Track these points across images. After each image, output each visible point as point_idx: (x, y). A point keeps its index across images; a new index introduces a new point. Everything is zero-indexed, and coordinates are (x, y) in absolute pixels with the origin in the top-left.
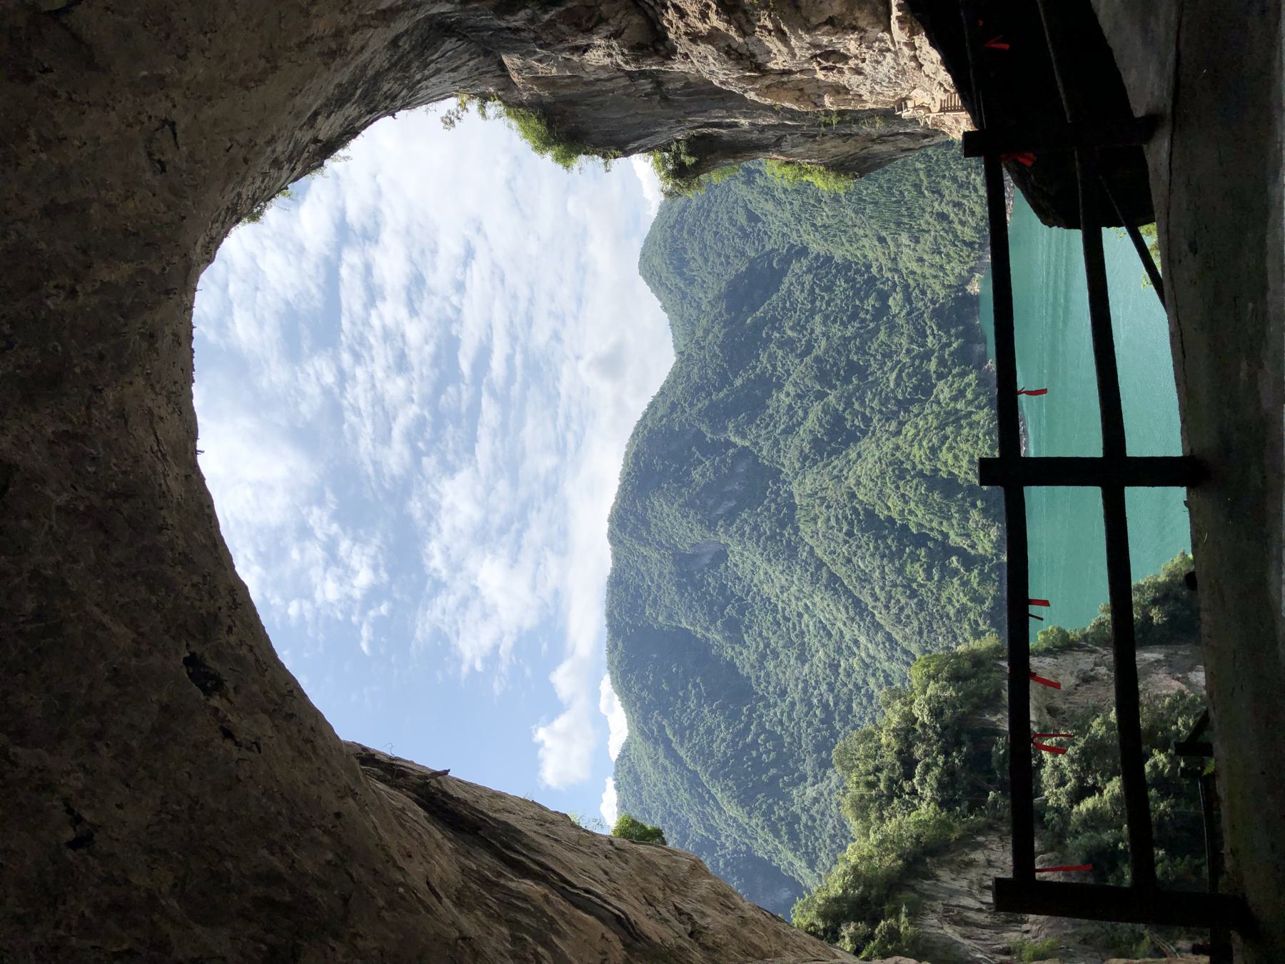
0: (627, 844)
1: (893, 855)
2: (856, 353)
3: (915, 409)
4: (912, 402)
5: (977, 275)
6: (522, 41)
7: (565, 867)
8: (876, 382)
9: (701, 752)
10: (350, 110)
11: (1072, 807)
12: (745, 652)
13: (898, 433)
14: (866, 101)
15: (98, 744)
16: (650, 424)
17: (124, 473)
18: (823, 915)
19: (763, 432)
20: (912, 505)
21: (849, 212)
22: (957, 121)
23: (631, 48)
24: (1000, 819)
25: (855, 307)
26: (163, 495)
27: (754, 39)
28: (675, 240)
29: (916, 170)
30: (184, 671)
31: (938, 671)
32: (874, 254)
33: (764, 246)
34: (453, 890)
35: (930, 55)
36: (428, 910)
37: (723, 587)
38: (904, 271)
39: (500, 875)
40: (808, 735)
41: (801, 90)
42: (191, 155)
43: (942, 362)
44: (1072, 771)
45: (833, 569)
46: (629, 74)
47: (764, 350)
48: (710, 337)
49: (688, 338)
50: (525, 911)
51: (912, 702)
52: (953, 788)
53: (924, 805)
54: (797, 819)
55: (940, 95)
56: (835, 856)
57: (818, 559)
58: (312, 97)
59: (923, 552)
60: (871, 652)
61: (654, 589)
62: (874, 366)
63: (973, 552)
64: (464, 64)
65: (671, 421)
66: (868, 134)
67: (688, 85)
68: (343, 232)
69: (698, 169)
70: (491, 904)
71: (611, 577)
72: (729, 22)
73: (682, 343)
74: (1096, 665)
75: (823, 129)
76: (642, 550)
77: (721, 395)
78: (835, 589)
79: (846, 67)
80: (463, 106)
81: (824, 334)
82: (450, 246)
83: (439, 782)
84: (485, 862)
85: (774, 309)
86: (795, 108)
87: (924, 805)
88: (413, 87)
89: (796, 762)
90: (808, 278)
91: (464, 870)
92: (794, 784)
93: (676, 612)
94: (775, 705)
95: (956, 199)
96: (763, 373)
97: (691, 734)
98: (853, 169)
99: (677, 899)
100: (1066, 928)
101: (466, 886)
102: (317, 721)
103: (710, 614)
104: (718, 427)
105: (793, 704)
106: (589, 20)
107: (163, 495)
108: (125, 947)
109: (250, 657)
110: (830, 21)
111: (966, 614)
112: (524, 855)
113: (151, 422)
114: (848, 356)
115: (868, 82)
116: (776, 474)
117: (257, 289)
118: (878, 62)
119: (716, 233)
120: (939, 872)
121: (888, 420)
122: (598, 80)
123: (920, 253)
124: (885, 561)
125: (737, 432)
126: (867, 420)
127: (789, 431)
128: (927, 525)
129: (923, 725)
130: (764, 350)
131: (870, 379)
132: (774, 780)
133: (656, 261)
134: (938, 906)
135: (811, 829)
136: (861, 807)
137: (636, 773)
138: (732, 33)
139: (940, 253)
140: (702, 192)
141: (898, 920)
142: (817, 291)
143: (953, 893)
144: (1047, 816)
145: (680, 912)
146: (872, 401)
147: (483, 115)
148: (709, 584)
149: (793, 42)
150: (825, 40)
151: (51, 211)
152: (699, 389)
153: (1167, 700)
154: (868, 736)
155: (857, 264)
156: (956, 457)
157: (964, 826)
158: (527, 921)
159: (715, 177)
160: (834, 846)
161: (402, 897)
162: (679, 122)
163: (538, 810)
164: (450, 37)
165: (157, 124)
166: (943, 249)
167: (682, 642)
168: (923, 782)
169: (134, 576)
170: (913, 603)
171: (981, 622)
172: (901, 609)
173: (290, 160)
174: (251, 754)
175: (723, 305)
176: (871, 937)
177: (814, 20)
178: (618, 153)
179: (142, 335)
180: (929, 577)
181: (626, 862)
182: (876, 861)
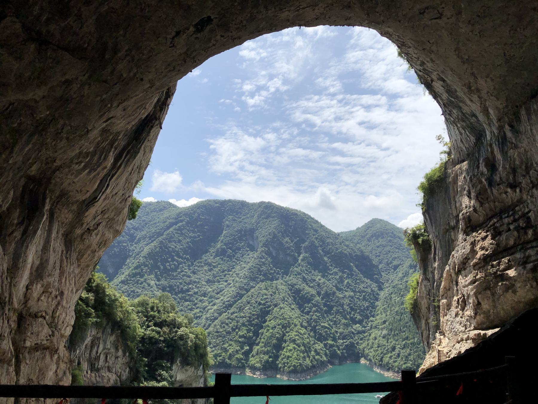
0: (128, 204)
3: (312, 334)
4: (315, 332)
5: (368, 363)
6: (473, 170)
7: (119, 176)
8: (324, 317)
9: (171, 237)
10: (445, 96)
12: (212, 257)
14: (443, 318)
18: (98, 286)
19: (304, 269)
20: (271, 331)
21: (397, 309)
22: (434, 357)
24: (136, 363)
25: (356, 310)
27: (472, 270)
29: (414, 338)
30: (205, 16)
31: (199, 339)
32: (379, 319)
34: (109, 128)
35: (464, 347)
36: (101, 116)
37: (239, 249)
38: (371, 331)
39: (116, 149)
41: (449, 290)
43: (331, 346)
46: (458, 216)
47: (339, 270)
49: (345, 238)
51: (187, 327)
52: (149, 344)
53: (143, 331)
54: (142, 276)
55: (445, 350)
56: (126, 292)
57: (250, 290)
58: (451, 78)
60: (210, 311)
61: (240, 220)
62: (331, 317)
64: (464, 145)
66: (430, 318)
67: (453, 241)
68: (393, 96)
69: (416, 244)
70: (103, 144)
71: (245, 202)
72: (480, 259)
75: (432, 299)
76: (256, 215)
77: (321, 251)
78: (237, 296)
79: (459, 309)
81: (345, 296)
82: (387, 141)
83: (157, 125)
84: (122, 142)
86: (442, 287)
88: (454, 123)
89: (165, 278)
91: (118, 133)
92: (156, 276)
93: (230, 228)
94: (190, 269)
95: (401, 355)
96: (329, 269)
97: (179, 233)
99: (104, 223)
101: (111, 134)
104: (307, 249)
105: (189, 277)
106: (482, 198)
109: (211, 45)
110: (479, 304)
111: (224, 352)
113: (312, 5)
114: (335, 306)
115: (452, 319)
116: (286, 273)
117: (370, 61)
118: (461, 324)
119: (389, 252)
120: (114, 335)
121: (308, 322)
122: (456, 202)
123: (378, 338)
124: (248, 318)
126: (308, 313)
127: (304, 280)
128: (263, 337)
129: (177, 332)
130: (339, 270)
131: (325, 315)
132: (158, 268)
133: (378, 225)
134: (100, 335)
136: (143, 304)
138: (475, 261)
139: (378, 347)
140: (406, 245)
141: (94, 317)
142: (364, 294)
143: (105, 342)
145: (98, 225)
146: (316, 315)
147: (442, 153)
148: (241, 243)
149: (470, 287)
150: (471, 301)
152: (323, 242)
154: (173, 308)
155: (375, 311)
156: (291, 350)
157: (133, 347)
158: (96, 159)
159: (413, 252)
161: (106, 106)
162: (437, 237)
164: (476, 139)
165: (440, 11)
167: (217, 230)
168: (153, 330)
171: (221, 358)
172: (227, 324)
173: (424, 69)
174: (169, 43)
175: (359, 253)
176: (88, 306)
177: (479, 296)
178: (424, 210)
180: (240, 337)
181: (120, 203)
182: (120, 309)
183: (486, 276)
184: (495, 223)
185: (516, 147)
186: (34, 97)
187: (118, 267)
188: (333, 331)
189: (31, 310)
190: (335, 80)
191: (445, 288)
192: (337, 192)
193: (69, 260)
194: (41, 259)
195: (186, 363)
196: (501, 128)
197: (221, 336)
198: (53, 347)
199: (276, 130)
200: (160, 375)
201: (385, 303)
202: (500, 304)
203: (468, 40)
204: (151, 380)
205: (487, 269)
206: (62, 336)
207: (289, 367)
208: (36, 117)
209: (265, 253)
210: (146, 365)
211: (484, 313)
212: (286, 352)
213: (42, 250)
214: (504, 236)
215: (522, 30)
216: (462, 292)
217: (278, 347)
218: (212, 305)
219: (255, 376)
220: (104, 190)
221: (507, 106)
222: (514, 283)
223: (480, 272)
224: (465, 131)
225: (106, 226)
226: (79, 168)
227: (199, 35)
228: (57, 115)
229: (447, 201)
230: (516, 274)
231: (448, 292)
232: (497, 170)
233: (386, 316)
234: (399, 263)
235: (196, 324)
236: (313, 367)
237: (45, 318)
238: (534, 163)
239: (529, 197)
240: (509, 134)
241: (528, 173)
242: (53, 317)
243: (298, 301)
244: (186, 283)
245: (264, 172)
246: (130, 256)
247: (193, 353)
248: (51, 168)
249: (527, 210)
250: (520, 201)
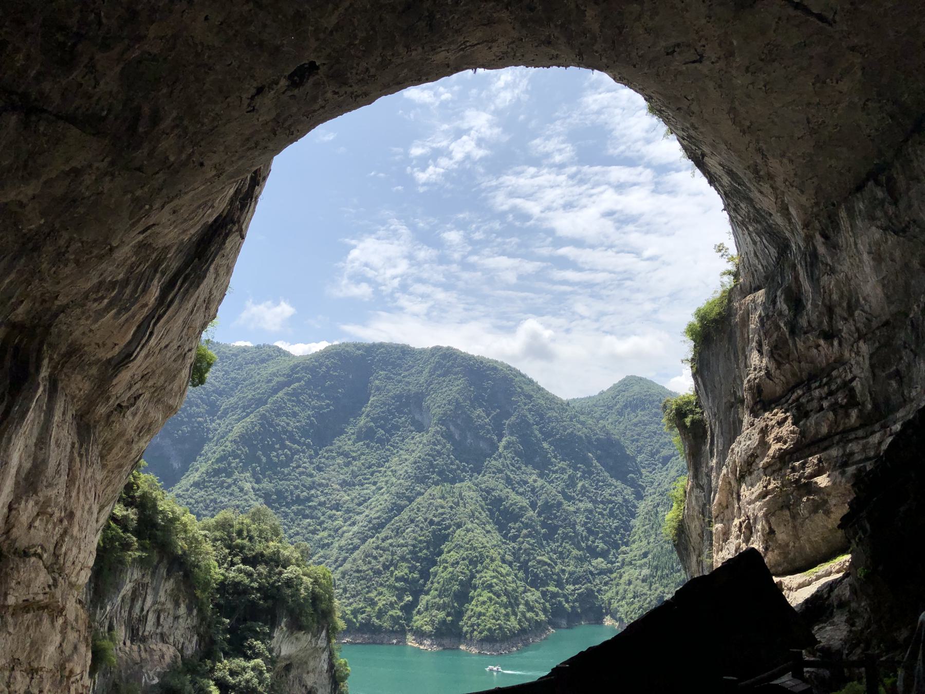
0: (189, 362)
2: (563, 532)
3: (521, 574)
4: (526, 572)
5: (617, 624)
7: (170, 319)
10: (726, 180)
11: (214, 680)
12: (350, 442)
16: (517, 379)
18: (144, 496)
19: (508, 462)
20: (450, 569)
23: (759, 386)
24: (209, 626)
25: (598, 533)
26: (433, 49)
31: (320, 585)
32: (635, 549)
33: (644, 468)
34: (151, 241)
36: (133, 225)
37: (397, 428)
38: (622, 570)
41: (727, 507)
42: (681, 73)
43: (554, 595)
44: (240, 681)
45: (407, 509)
47: (568, 465)
48: (579, 426)
49: (578, 409)
50: (135, 291)
51: (299, 566)
52: (233, 593)
54: (229, 475)
56: (201, 502)
57: (415, 498)
59: (416, 575)
60: (346, 534)
61: (399, 378)
62: (554, 546)
63: (415, 612)
64: (759, 261)
65: (519, 395)
69: (682, 427)
70: (142, 266)
71: (408, 347)
72: (773, 457)
75: (707, 520)
77: (537, 432)
78: (392, 509)
80: (731, 259)
82: (652, 245)
84: (173, 263)
87: (222, 571)
89: (270, 477)
90: (619, 499)
91: (166, 249)
92: (254, 475)
93: (382, 391)
94: (312, 463)
97: (293, 401)
99: (147, 395)
101: (154, 250)
102: (273, 150)
105: (311, 476)
107: (433, 49)
108: (104, 21)
109: (316, 107)
110: (772, 532)
111: (370, 605)
112: (179, 289)
114: (561, 526)
116: (478, 470)
117: (624, 109)
119: (655, 433)
120: (172, 580)
121: (513, 553)
123: (634, 582)
124: (410, 548)
125: (509, 443)
126: (514, 539)
127: (509, 481)
128: (436, 580)
129: (281, 573)
130: (568, 465)
131: (544, 542)
132: (259, 460)
133: (636, 388)
134: (147, 579)
135: (221, 485)
136: (224, 525)
137: (268, 360)
138: (766, 460)
139: (634, 597)
141: (137, 550)
142: (610, 506)
143: (156, 591)
144: (208, 662)
145: (137, 398)
146: (528, 543)
147: (724, 274)
149: (758, 503)
150: (759, 527)
152: (542, 416)
155: (629, 535)
156: (484, 603)
157: (205, 600)
158: (128, 292)
160: (208, 501)
165: (700, 50)
167: (359, 396)
168: (240, 571)
170: (380, 567)
172: (375, 558)
174: (245, 106)
175: (602, 436)
176: (125, 530)
177: (773, 520)
179: (549, 36)
180: (398, 579)
181: (175, 361)
182: (182, 535)
183: (783, 485)
184: (800, 397)
185: (833, 271)
186: (19, 198)
188: (557, 569)
189: (17, 545)
190: (563, 142)
191: (720, 504)
192: (568, 331)
193: (84, 460)
194: (35, 459)
195: (296, 626)
196: (809, 239)
197: (364, 579)
198: (55, 604)
199: (460, 226)
200: (251, 647)
201: (647, 522)
202: (804, 533)
203: (749, 96)
204: (236, 656)
206: (72, 585)
207: (480, 633)
208: (22, 229)
209: (442, 436)
210: (227, 631)
211: (780, 547)
212: (477, 605)
213: (36, 445)
214: (812, 420)
215: (835, 81)
216: (746, 513)
217: (463, 597)
219: (422, 647)
220: (144, 341)
221: (817, 204)
222: (826, 497)
223: (774, 480)
224: (761, 239)
225: (150, 400)
226: (99, 308)
227: (296, 92)
228: (57, 226)
230: (830, 484)
231: (726, 512)
232: (804, 307)
233: (648, 543)
234: (671, 452)
235: (321, 557)
236: (523, 631)
237: (40, 557)
238: (861, 299)
239: (853, 355)
240: (821, 250)
241: (851, 315)
242: (56, 555)
244: (305, 486)
245: (441, 295)
246: (210, 440)
247: (310, 610)
248: (49, 309)
249: (849, 376)
250: (840, 362)
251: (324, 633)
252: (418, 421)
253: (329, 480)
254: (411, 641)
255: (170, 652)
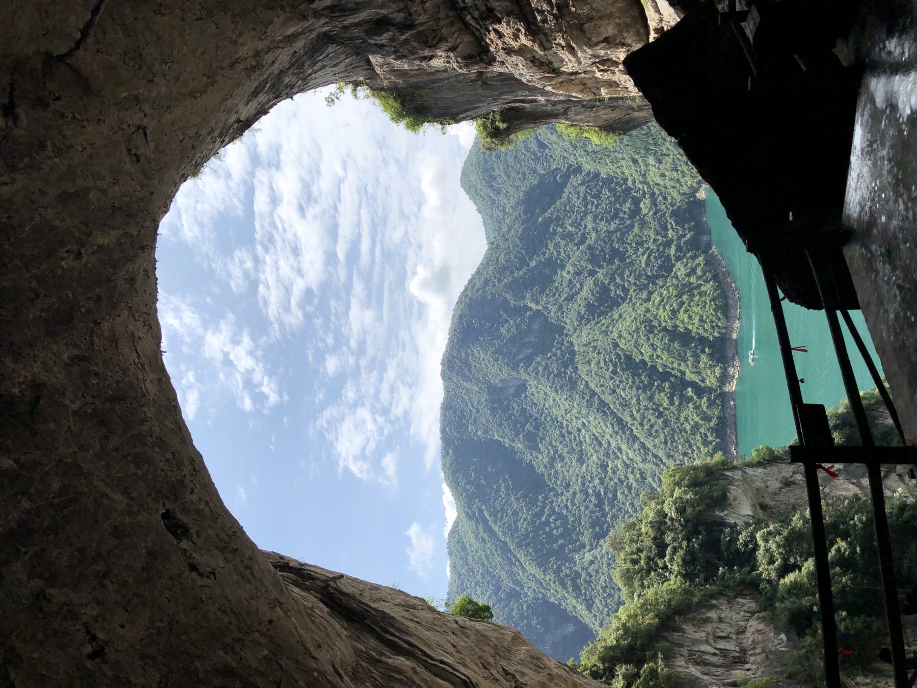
0: (468, 623)
1: (651, 615)
8: (632, 263)
9: (509, 528)
10: (262, 98)
12: (540, 457)
13: (648, 299)
15: (106, 582)
17: (118, 382)
18: (603, 659)
19: (552, 299)
20: (659, 351)
23: (464, 58)
24: (728, 587)
25: (616, 209)
26: (144, 395)
27: (551, 52)
28: (486, 162)
30: (162, 523)
32: (629, 171)
33: (550, 166)
34: (350, 668)
38: (651, 183)
39: (382, 654)
40: (586, 515)
41: (584, 84)
42: (157, 148)
43: (679, 249)
44: (779, 553)
45: (602, 397)
47: (551, 241)
49: (496, 233)
51: (663, 502)
54: (578, 575)
57: (591, 390)
61: (474, 411)
62: (631, 251)
63: (703, 385)
64: (341, 62)
69: (509, 131)
71: (443, 404)
72: (534, 41)
73: (492, 235)
74: (794, 473)
75: (598, 103)
77: (521, 273)
78: (604, 412)
80: (340, 89)
81: (594, 229)
84: (371, 644)
85: (558, 211)
87: (673, 577)
90: (582, 189)
92: (577, 550)
94: (562, 494)
96: (551, 257)
97: (502, 515)
98: (618, 129)
99: (504, 663)
100: (776, 667)
101: (358, 664)
103: (515, 429)
105: (575, 494)
109: (207, 510)
110: (606, 40)
112: (396, 636)
113: (133, 343)
114: (611, 245)
116: (560, 329)
119: (516, 157)
120: (684, 627)
121: (640, 290)
125: (532, 300)
126: (626, 291)
127: (570, 298)
128: (670, 365)
129: (672, 519)
130: (551, 241)
131: (628, 261)
132: (562, 547)
133: (473, 177)
134: (684, 651)
136: (628, 577)
137: (463, 543)
138: (536, 48)
139: (677, 170)
141: (656, 663)
142: (589, 198)
144: (761, 586)
145: (507, 673)
146: (629, 276)
147: (356, 96)
148: (514, 408)
149: (579, 54)
150: (602, 52)
151: (65, 198)
152: (505, 269)
153: (847, 502)
155: (617, 178)
156: (690, 317)
157: (702, 593)
159: (520, 137)
160: (605, 595)
163: (403, 597)
165: (133, 129)
166: (679, 168)
167: (493, 450)
168: (672, 560)
169: (126, 457)
170: (660, 421)
172: (652, 426)
174: (209, 581)
176: (638, 675)
177: (594, 40)
178: (451, 121)
179: (125, 280)
180: (672, 403)
181: (468, 637)
183: (561, 31)
184: (473, 17)
187: (563, 616)
188: (653, 247)
191: (582, 91)
195: (722, 501)
196: (317, 14)
199: (320, 358)
200: (746, 544)
201: (603, 161)
202: (605, 9)
203: (178, 79)
204: (755, 560)
205: (550, 29)
207: (719, 319)
209: (529, 366)
210: (731, 570)
211: (620, 32)
217: (685, 338)
218: (621, 453)
219: (737, 376)
227: (193, 531)
229: (435, 85)
232: (385, 16)
235: (654, 479)
236: (715, 277)
243: (606, 307)
246: (544, 596)
247: (706, 488)
251: (728, 473)
252: (516, 390)
253: (577, 475)
254: (731, 387)
255: (754, 625)
